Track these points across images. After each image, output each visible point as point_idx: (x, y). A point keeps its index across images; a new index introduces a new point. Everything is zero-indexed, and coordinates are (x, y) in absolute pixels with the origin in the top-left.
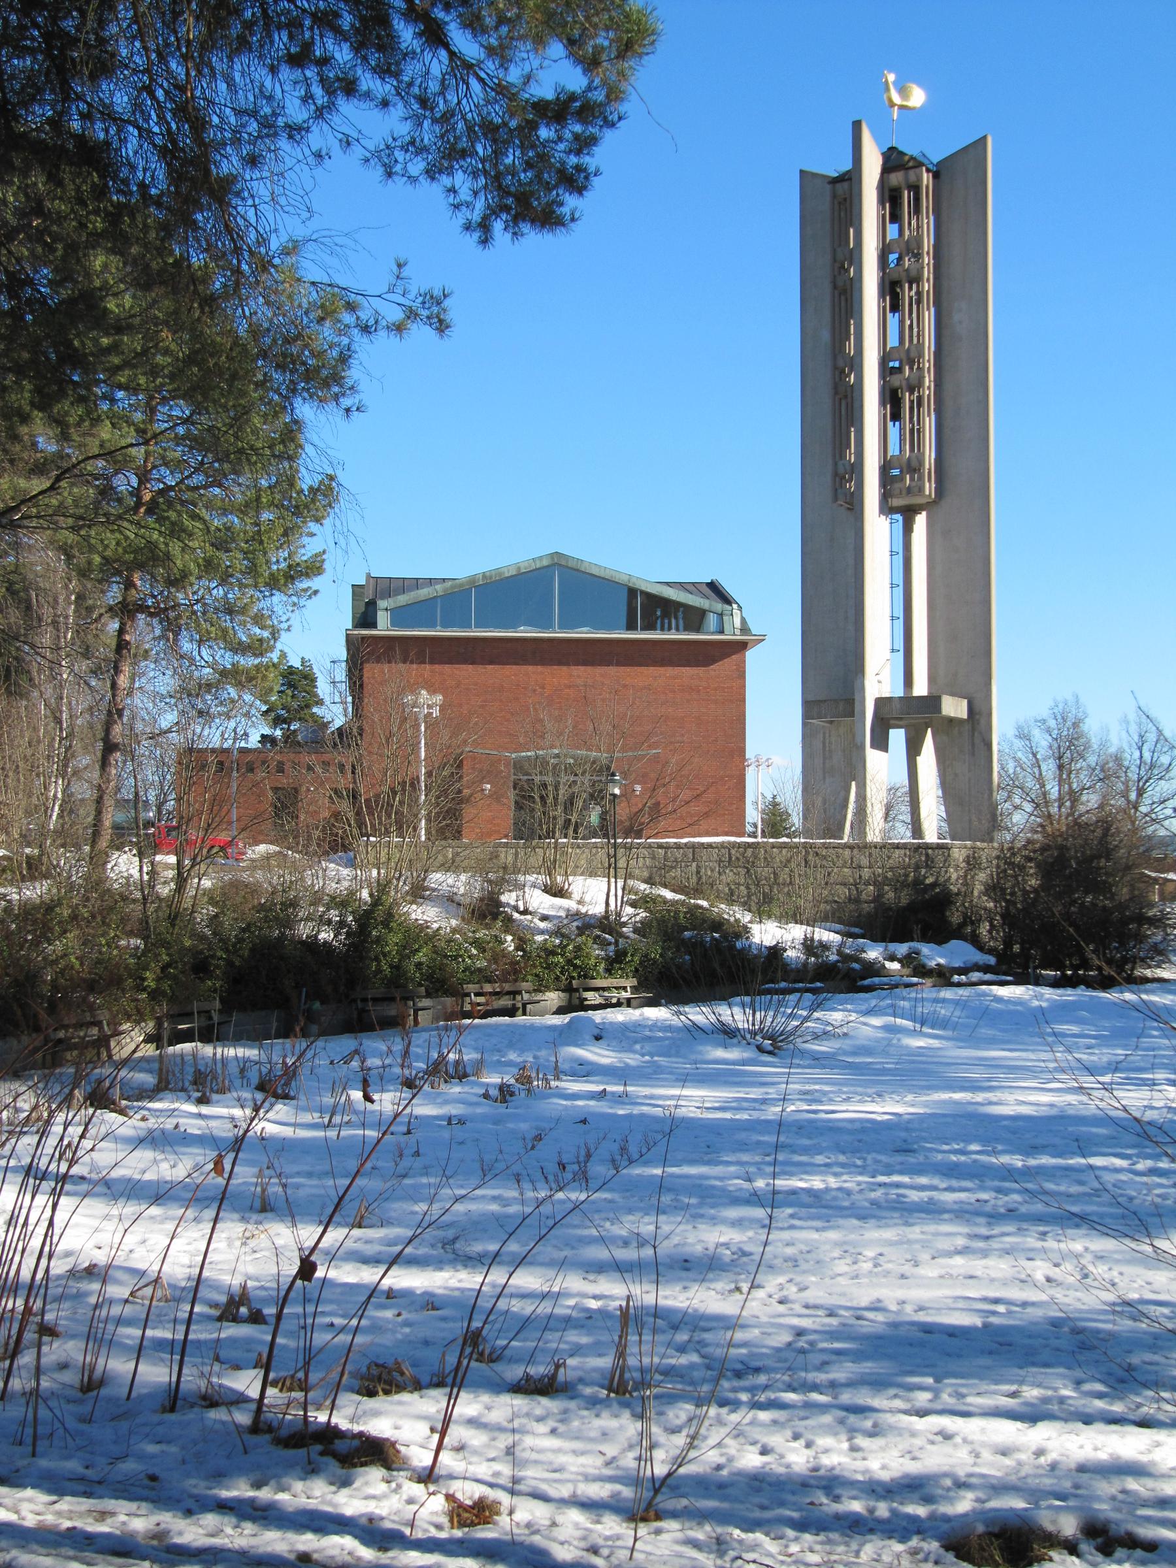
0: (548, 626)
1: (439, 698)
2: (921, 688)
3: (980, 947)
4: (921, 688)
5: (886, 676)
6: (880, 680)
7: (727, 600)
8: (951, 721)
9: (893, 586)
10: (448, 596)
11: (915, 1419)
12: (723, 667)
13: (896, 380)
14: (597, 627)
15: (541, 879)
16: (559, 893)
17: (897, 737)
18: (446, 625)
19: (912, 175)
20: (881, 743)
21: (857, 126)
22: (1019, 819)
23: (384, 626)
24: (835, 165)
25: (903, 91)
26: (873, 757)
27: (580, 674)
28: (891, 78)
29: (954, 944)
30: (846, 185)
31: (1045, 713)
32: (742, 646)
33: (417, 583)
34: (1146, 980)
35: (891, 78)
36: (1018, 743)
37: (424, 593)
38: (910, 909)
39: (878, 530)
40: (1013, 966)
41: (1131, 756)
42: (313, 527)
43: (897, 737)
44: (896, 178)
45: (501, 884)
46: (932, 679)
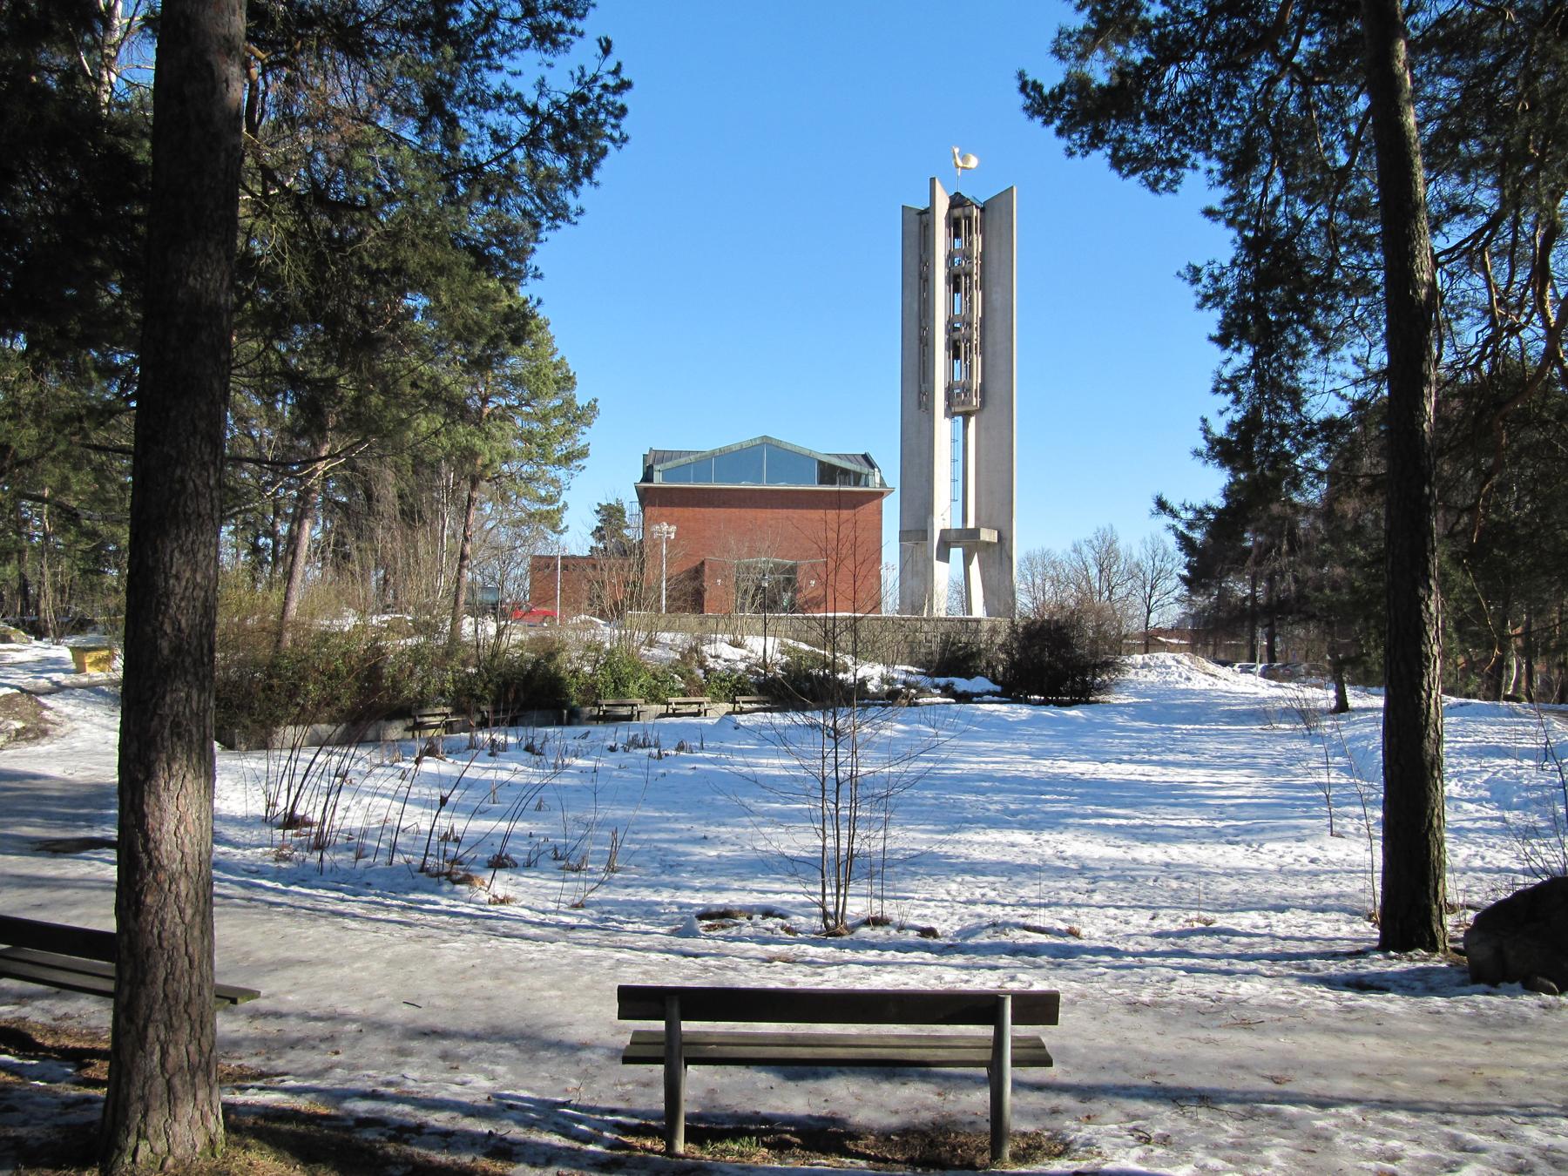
0: (759, 481)
1: (673, 528)
2: (971, 524)
3: (995, 681)
4: (971, 524)
5: (947, 516)
6: (945, 516)
7: (872, 465)
8: (988, 543)
9: (954, 461)
10: (698, 462)
11: (1310, 1110)
12: (871, 506)
13: (956, 335)
14: (790, 482)
15: (727, 637)
16: (737, 645)
17: (956, 553)
18: (696, 481)
19: (967, 211)
20: (944, 557)
21: (933, 180)
22: (1024, 602)
23: (658, 481)
24: (923, 204)
25: (964, 159)
26: (939, 566)
27: (749, 513)
28: (957, 150)
29: (978, 678)
30: (926, 216)
31: (1091, 536)
32: (881, 495)
33: (680, 454)
34: (1097, 702)
35: (957, 150)
36: (1073, 555)
37: (683, 460)
38: (953, 662)
39: (944, 429)
40: (1012, 690)
41: (1147, 565)
42: (585, 429)
43: (956, 553)
44: (957, 212)
45: (701, 640)
46: (977, 518)
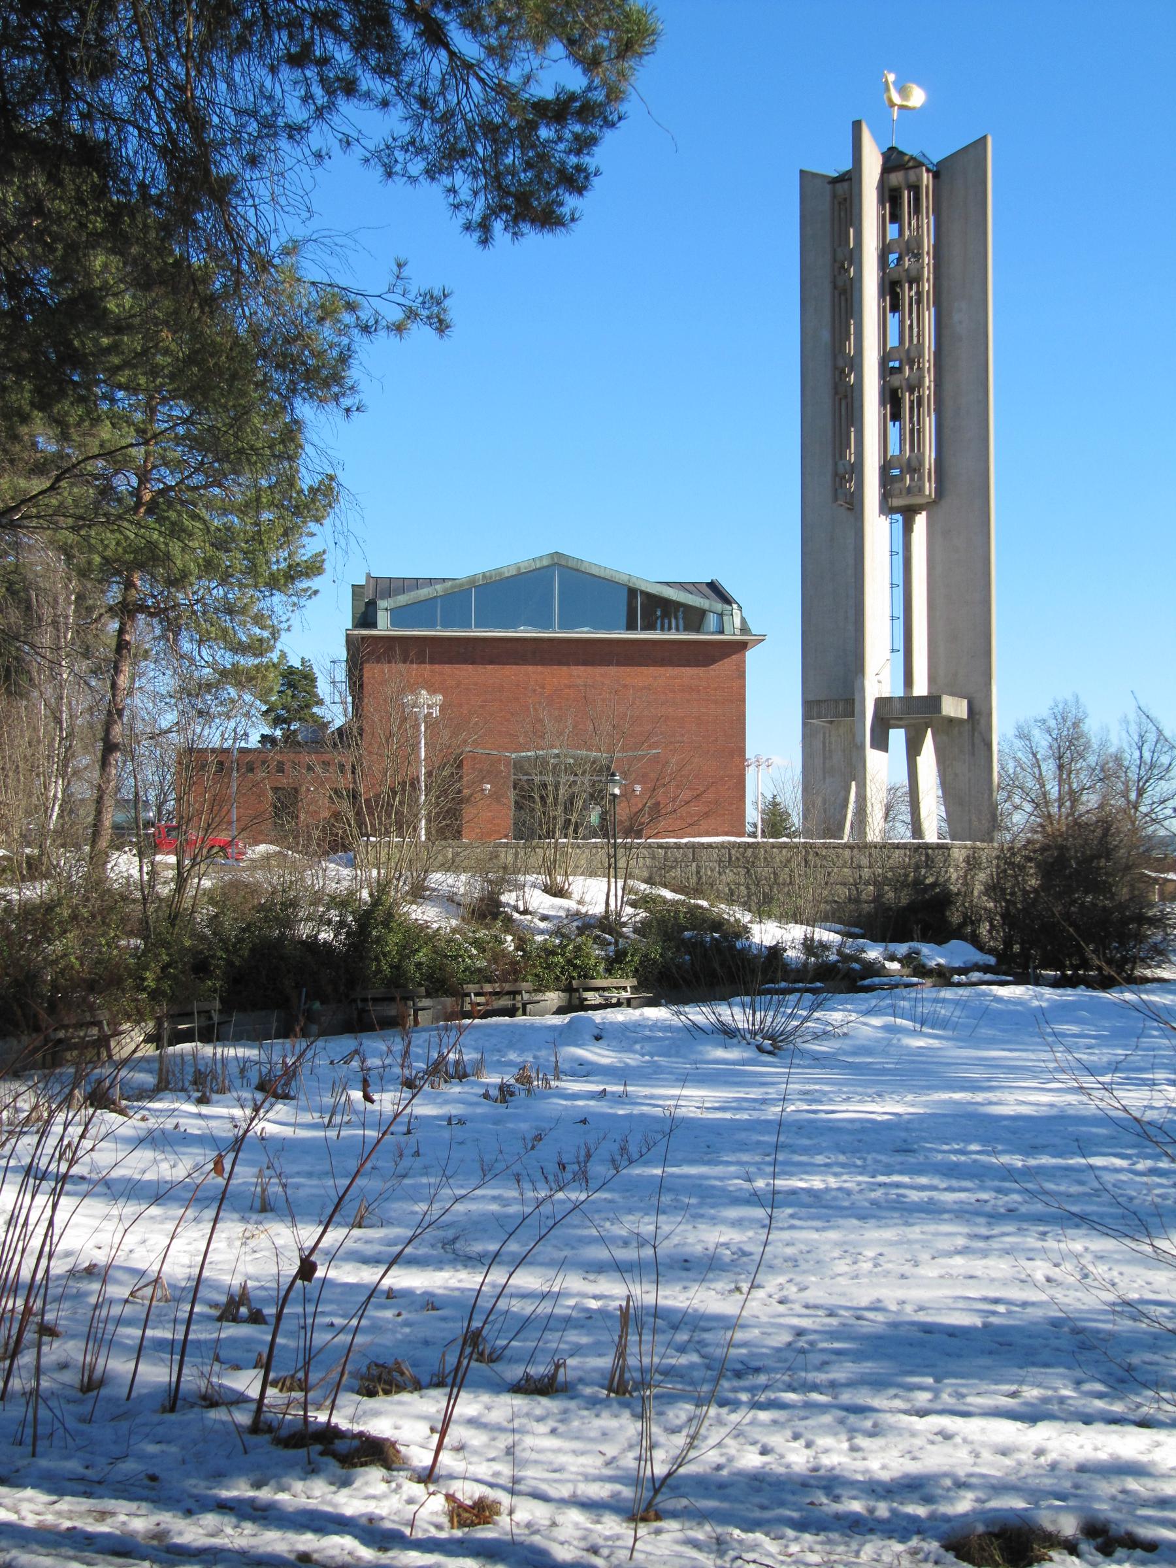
0: (548, 626)
1: (439, 698)
2: (921, 688)
3: (980, 947)
4: (921, 688)
5: (886, 676)
6: (880, 680)
7: (727, 600)
8: (951, 721)
9: (893, 586)
10: (448, 596)
11: (915, 1419)
12: (723, 667)
13: (896, 380)
14: (597, 627)
15: (541, 879)
16: (559, 893)
17: (897, 737)
18: (446, 625)
19: (912, 175)
20: (881, 743)
21: (857, 126)
22: (1019, 819)
23: (384, 626)
24: (835, 165)
25: (903, 91)
26: (873, 757)
27: (580, 674)
28: (891, 78)
29: (954, 944)
30: (846, 185)
31: (1045, 713)
32: (742, 646)
33: (417, 583)
34: (1146, 980)
35: (891, 78)
36: (1018, 743)
37: (424, 593)
38: (910, 909)
39: (878, 530)
40: (1013, 966)
41: (1131, 756)
42: (313, 527)
43: (897, 737)
44: (896, 178)
45: (501, 884)
46: (932, 679)
